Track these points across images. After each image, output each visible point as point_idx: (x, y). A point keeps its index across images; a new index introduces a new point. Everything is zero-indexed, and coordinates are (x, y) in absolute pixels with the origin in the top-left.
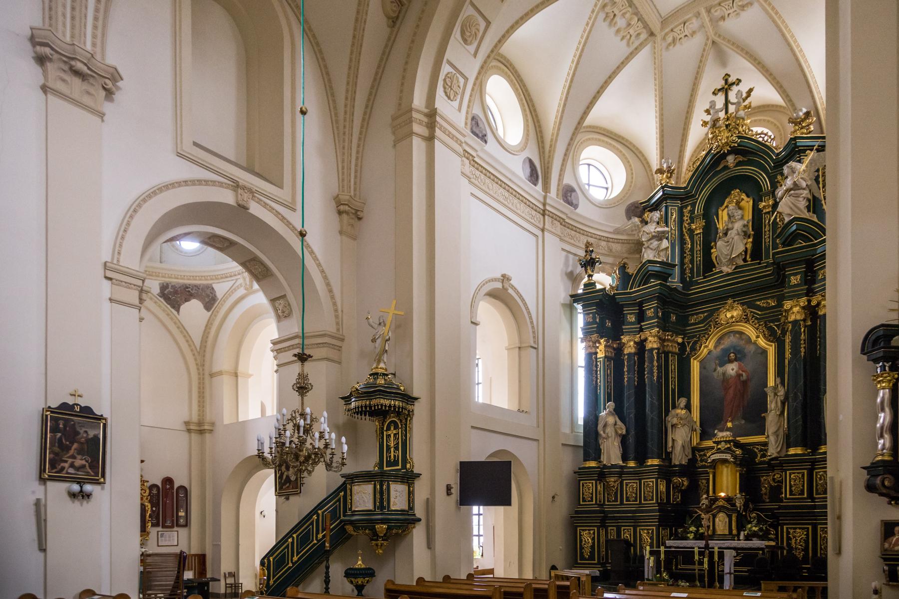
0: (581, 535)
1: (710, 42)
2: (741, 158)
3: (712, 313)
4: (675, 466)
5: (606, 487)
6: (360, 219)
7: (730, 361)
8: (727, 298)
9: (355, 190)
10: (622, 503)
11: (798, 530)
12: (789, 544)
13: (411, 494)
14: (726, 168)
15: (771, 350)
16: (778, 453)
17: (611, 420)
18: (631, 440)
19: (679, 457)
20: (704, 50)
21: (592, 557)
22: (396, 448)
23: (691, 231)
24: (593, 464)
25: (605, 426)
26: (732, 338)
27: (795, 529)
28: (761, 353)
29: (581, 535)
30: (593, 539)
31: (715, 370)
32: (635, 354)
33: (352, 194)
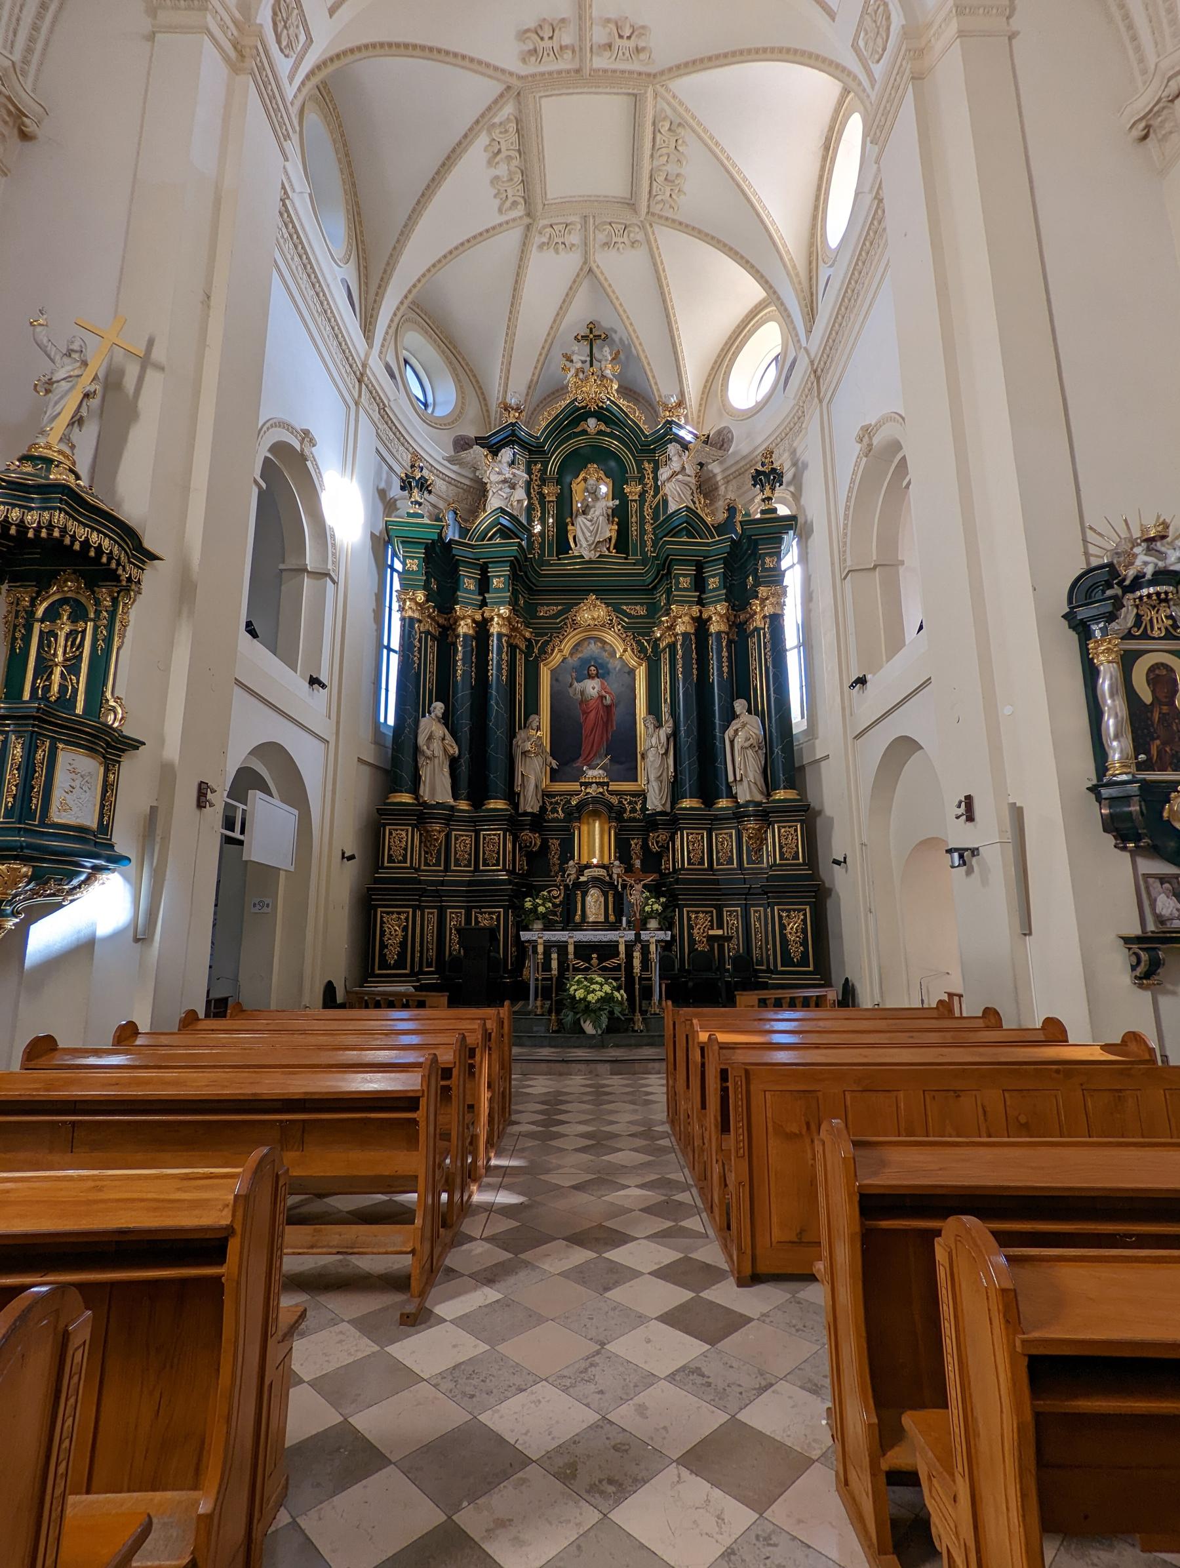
0: (382, 922)
1: (586, 269)
2: (603, 427)
3: (568, 608)
4: (526, 814)
5: (426, 840)
6: (25, 136)
7: (590, 677)
8: (588, 592)
9: (29, 50)
10: (477, 869)
11: (701, 915)
12: (690, 935)
13: (108, 788)
14: (584, 432)
15: (641, 674)
16: (663, 805)
17: (439, 730)
18: (464, 768)
19: (530, 803)
20: (578, 275)
21: (400, 964)
22: (72, 667)
23: (542, 496)
24: (406, 798)
25: (430, 738)
26: (592, 646)
27: (697, 912)
28: (629, 673)
29: (382, 922)
30: (405, 929)
31: (571, 685)
32: (473, 637)
33: (17, 57)
